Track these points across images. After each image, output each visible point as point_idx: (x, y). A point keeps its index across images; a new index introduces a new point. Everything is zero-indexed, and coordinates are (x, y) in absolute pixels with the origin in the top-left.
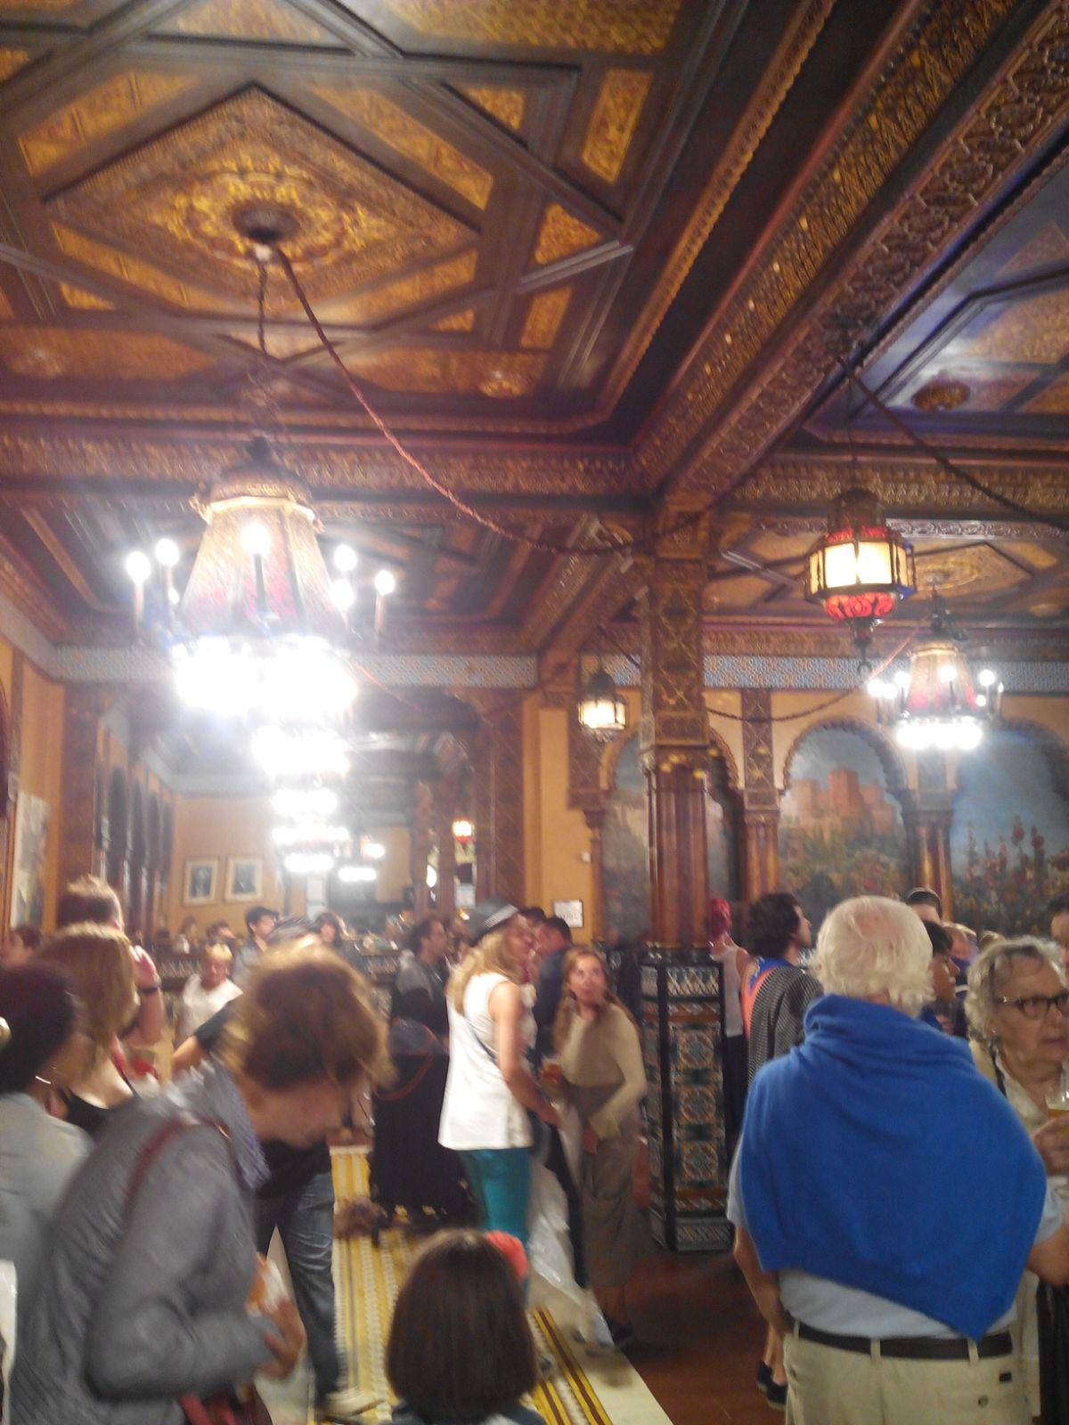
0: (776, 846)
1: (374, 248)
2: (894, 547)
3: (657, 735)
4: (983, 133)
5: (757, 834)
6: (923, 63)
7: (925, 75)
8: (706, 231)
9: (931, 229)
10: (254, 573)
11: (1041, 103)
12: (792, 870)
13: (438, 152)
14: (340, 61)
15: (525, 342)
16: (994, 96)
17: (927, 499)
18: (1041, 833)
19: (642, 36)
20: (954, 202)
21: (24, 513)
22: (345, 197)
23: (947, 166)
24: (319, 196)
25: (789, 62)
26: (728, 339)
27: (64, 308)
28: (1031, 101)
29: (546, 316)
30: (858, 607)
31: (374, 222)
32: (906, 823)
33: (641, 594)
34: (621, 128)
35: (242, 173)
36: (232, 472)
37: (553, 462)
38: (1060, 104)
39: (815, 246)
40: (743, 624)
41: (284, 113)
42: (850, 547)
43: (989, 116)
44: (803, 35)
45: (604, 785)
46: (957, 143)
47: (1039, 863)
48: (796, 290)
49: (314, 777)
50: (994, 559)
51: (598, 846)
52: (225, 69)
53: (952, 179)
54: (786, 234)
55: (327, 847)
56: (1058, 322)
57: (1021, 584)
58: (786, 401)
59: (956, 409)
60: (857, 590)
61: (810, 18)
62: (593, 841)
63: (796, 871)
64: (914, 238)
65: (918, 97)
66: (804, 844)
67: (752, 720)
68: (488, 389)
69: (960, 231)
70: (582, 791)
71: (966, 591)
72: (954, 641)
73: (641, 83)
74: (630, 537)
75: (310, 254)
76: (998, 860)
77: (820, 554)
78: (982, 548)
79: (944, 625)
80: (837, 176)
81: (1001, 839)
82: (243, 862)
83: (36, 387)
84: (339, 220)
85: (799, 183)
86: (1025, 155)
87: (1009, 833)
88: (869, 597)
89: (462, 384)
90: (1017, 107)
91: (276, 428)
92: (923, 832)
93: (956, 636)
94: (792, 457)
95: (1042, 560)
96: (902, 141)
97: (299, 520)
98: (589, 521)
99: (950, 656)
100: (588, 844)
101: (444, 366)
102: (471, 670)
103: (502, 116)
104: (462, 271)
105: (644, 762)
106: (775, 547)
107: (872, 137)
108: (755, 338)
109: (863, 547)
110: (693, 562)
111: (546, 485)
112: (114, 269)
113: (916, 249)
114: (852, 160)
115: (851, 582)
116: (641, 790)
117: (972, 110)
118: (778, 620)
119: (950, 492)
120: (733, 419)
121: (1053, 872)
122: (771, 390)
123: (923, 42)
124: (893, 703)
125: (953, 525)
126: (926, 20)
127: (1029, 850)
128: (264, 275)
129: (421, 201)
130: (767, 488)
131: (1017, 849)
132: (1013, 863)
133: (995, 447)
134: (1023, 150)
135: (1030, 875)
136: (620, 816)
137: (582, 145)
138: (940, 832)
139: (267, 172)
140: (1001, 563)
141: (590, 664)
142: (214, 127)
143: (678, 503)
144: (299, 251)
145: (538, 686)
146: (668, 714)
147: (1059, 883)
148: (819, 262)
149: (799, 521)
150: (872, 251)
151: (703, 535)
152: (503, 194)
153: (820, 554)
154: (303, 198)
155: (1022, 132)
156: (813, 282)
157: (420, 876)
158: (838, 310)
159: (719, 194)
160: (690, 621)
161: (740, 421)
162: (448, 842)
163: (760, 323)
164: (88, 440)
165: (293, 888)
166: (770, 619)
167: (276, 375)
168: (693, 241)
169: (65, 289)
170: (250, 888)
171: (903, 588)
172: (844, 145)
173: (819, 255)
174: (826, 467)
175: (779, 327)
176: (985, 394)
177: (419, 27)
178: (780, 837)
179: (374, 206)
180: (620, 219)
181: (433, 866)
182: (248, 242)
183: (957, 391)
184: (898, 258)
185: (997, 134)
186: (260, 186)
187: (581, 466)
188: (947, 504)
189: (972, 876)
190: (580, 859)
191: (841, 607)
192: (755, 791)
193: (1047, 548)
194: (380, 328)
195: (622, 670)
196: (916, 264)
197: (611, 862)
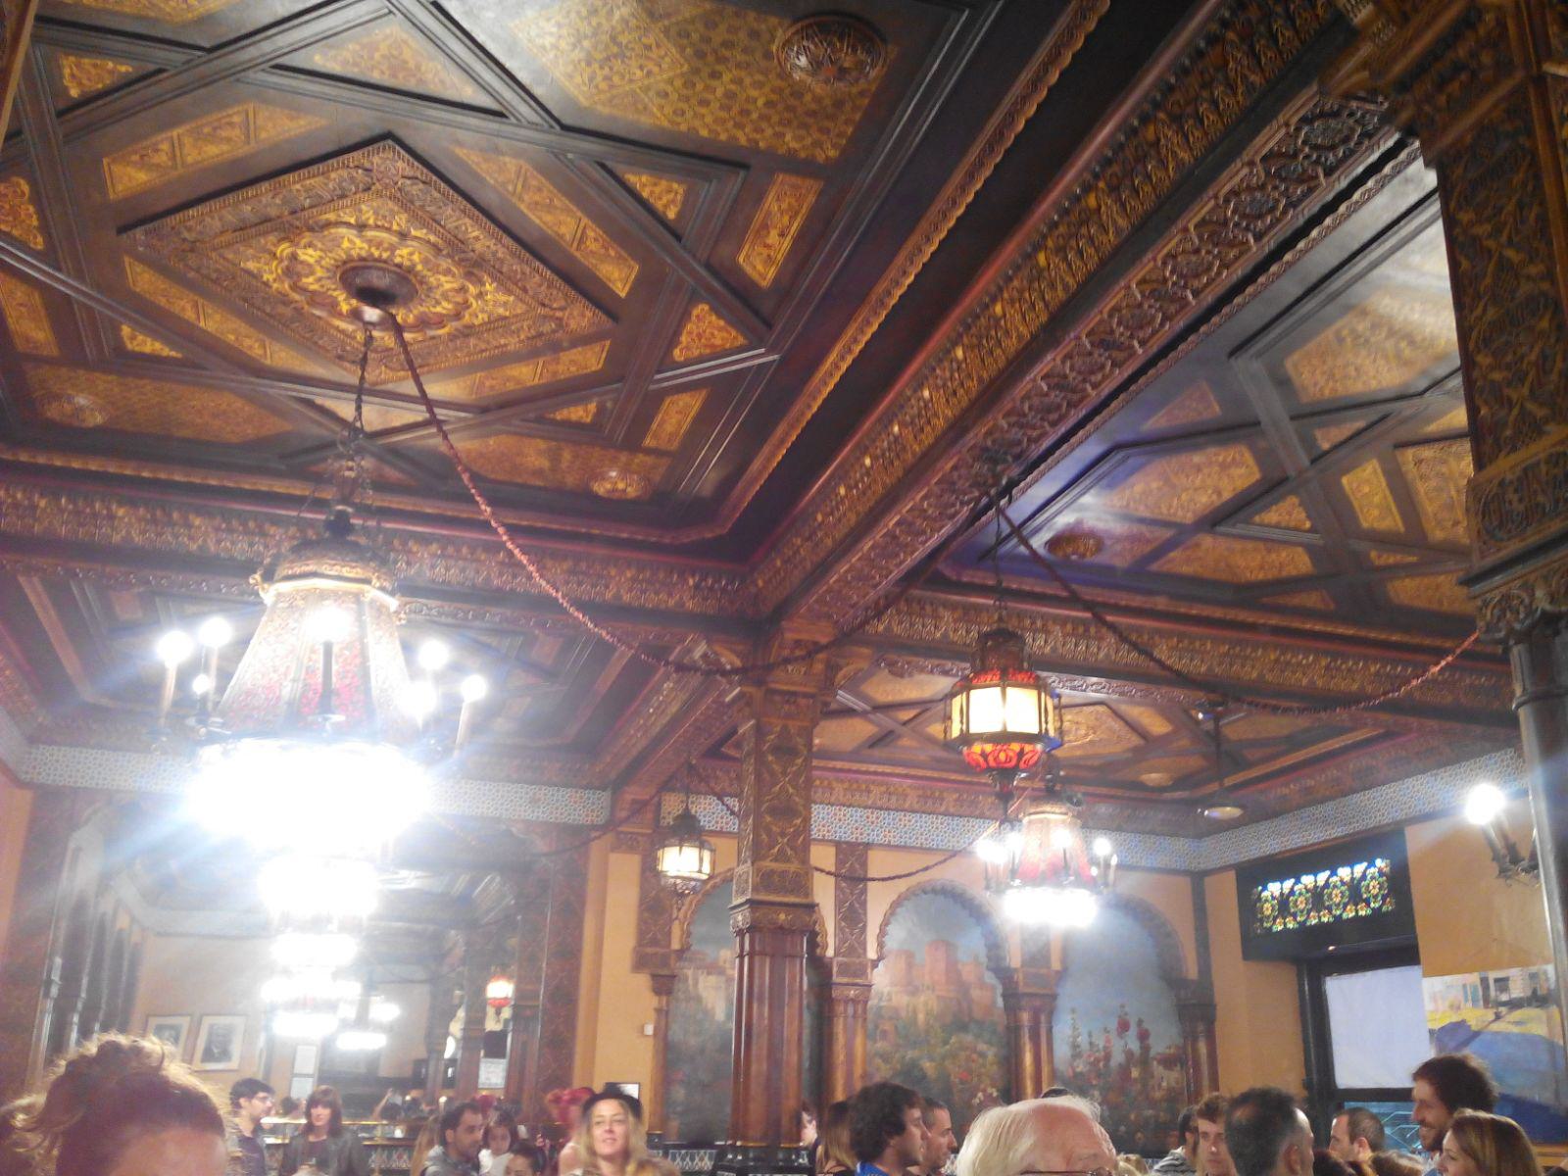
0: (864, 1027)
1: (496, 324)
2: (1043, 695)
3: (755, 889)
4: (1157, 281)
5: (846, 1010)
6: (1099, 207)
7: (1100, 218)
8: (857, 349)
9: (1092, 372)
10: (320, 665)
11: (1218, 256)
12: (881, 1056)
13: (584, 232)
14: (492, 125)
15: (649, 442)
16: (1173, 243)
17: (1054, 650)
18: (1145, 1025)
19: (817, 144)
20: (1120, 347)
21: (21, 579)
22: (474, 267)
23: (1116, 309)
24: (445, 263)
25: (963, 189)
26: (868, 462)
27: (120, 349)
28: (1209, 252)
29: (676, 416)
30: (1002, 756)
31: (502, 297)
32: (1006, 1008)
33: (747, 727)
34: (782, 235)
35: (361, 227)
36: (306, 546)
37: (661, 575)
38: (1237, 258)
39: (969, 376)
40: (841, 770)
41: (420, 171)
42: (998, 690)
43: (1165, 263)
44: (980, 164)
45: (676, 945)
46: (1129, 288)
47: (1144, 1061)
48: (946, 418)
49: (329, 920)
50: (1110, 720)
51: (663, 1015)
52: (361, 115)
53: (1119, 323)
54: (941, 361)
55: (332, 1006)
56: (1198, 482)
57: (1135, 750)
58: (924, 532)
59: (1089, 559)
60: (1003, 738)
61: (990, 147)
62: (658, 1011)
63: (886, 1058)
64: (1074, 379)
65: (1091, 239)
66: (896, 1027)
67: (845, 878)
68: (601, 488)
69: (1120, 376)
70: (649, 950)
71: (1078, 753)
72: (1068, 805)
73: (809, 191)
74: (738, 663)
75: (423, 323)
76: (1103, 1053)
77: (964, 695)
78: (1101, 709)
79: (1058, 788)
80: (998, 309)
81: (1106, 1031)
82: (222, 1021)
83: (73, 437)
84: (463, 289)
85: (957, 313)
86: (1195, 305)
87: (1113, 1025)
88: (1016, 747)
89: (571, 481)
90: (1194, 258)
91: (366, 511)
92: (1025, 1017)
93: (1070, 799)
94: (928, 594)
95: (1158, 726)
96: (1071, 281)
97: (380, 610)
98: (695, 642)
99: (1063, 822)
100: (652, 1015)
101: (555, 459)
102: (534, 801)
103: (659, 205)
104: (591, 359)
105: (736, 921)
106: (887, 689)
107: (1039, 274)
108: (896, 463)
109: (1010, 690)
110: (806, 695)
111: (652, 599)
112: (189, 314)
113: (1074, 391)
114: (1016, 294)
115: (997, 728)
116: (727, 955)
117: (1150, 255)
118: (880, 769)
119: (1076, 645)
120: (867, 545)
121: (1158, 1070)
122: (910, 519)
123: (1101, 185)
124: (1002, 868)
125: (1078, 681)
126: (1108, 162)
127: (1134, 1046)
128: (370, 339)
129: (559, 282)
130: (892, 624)
131: (1122, 1043)
132: (1118, 1058)
133: (1123, 603)
134: (1194, 303)
135: (1135, 1073)
136: (690, 982)
137: (740, 248)
138: (1043, 1018)
139: (388, 230)
140: (1117, 725)
141: (672, 806)
142: (337, 175)
143: (796, 630)
144: (411, 319)
145: (610, 826)
146: (768, 864)
147: (1164, 1084)
148: (974, 394)
149: (921, 661)
150: (1029, 386)
151: (819, 667)
152: (647, 284)
153: (964, 695)
154: (425, 262)
155: (1196, 284)
156: (965, 412)
157: (435, 1044)
158: (989, 443)
159: (876, 314)
160: (799, 761)
161: (873, 547)
162: (478, 1007)
163: (904, 448)
164: (120, 504)
165: (279, 1057)
166: (873, 768)
167: (360, 451)
168: (843, 358)
169: (126, 330)
170: (225, 1055)
171: (1049, 739)
172: (1010, 279)
173: (973, 385)
174: (954, 607)
175: (925, 455)
176: (1118, 547)
177: (584, 102)
178: (870, 1016)
179: (504, 280)
180: (769, 325)
181: (455, 1038)
182: (354, 302)
183: (1091, 542)
184: (1056, 397)
185: (1170, 283)
186: (379, 245)
187: (691, 582)
188: (1085, 659)
189: (1074, 1071)
190: (642, 1029)
191: (983, 754)
192: (845, 959)
193: (1164, 712)
194: (489, 410)
195: (709, 811)
196: (1071, 405)
197: (676, 1033)
